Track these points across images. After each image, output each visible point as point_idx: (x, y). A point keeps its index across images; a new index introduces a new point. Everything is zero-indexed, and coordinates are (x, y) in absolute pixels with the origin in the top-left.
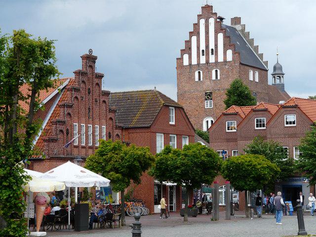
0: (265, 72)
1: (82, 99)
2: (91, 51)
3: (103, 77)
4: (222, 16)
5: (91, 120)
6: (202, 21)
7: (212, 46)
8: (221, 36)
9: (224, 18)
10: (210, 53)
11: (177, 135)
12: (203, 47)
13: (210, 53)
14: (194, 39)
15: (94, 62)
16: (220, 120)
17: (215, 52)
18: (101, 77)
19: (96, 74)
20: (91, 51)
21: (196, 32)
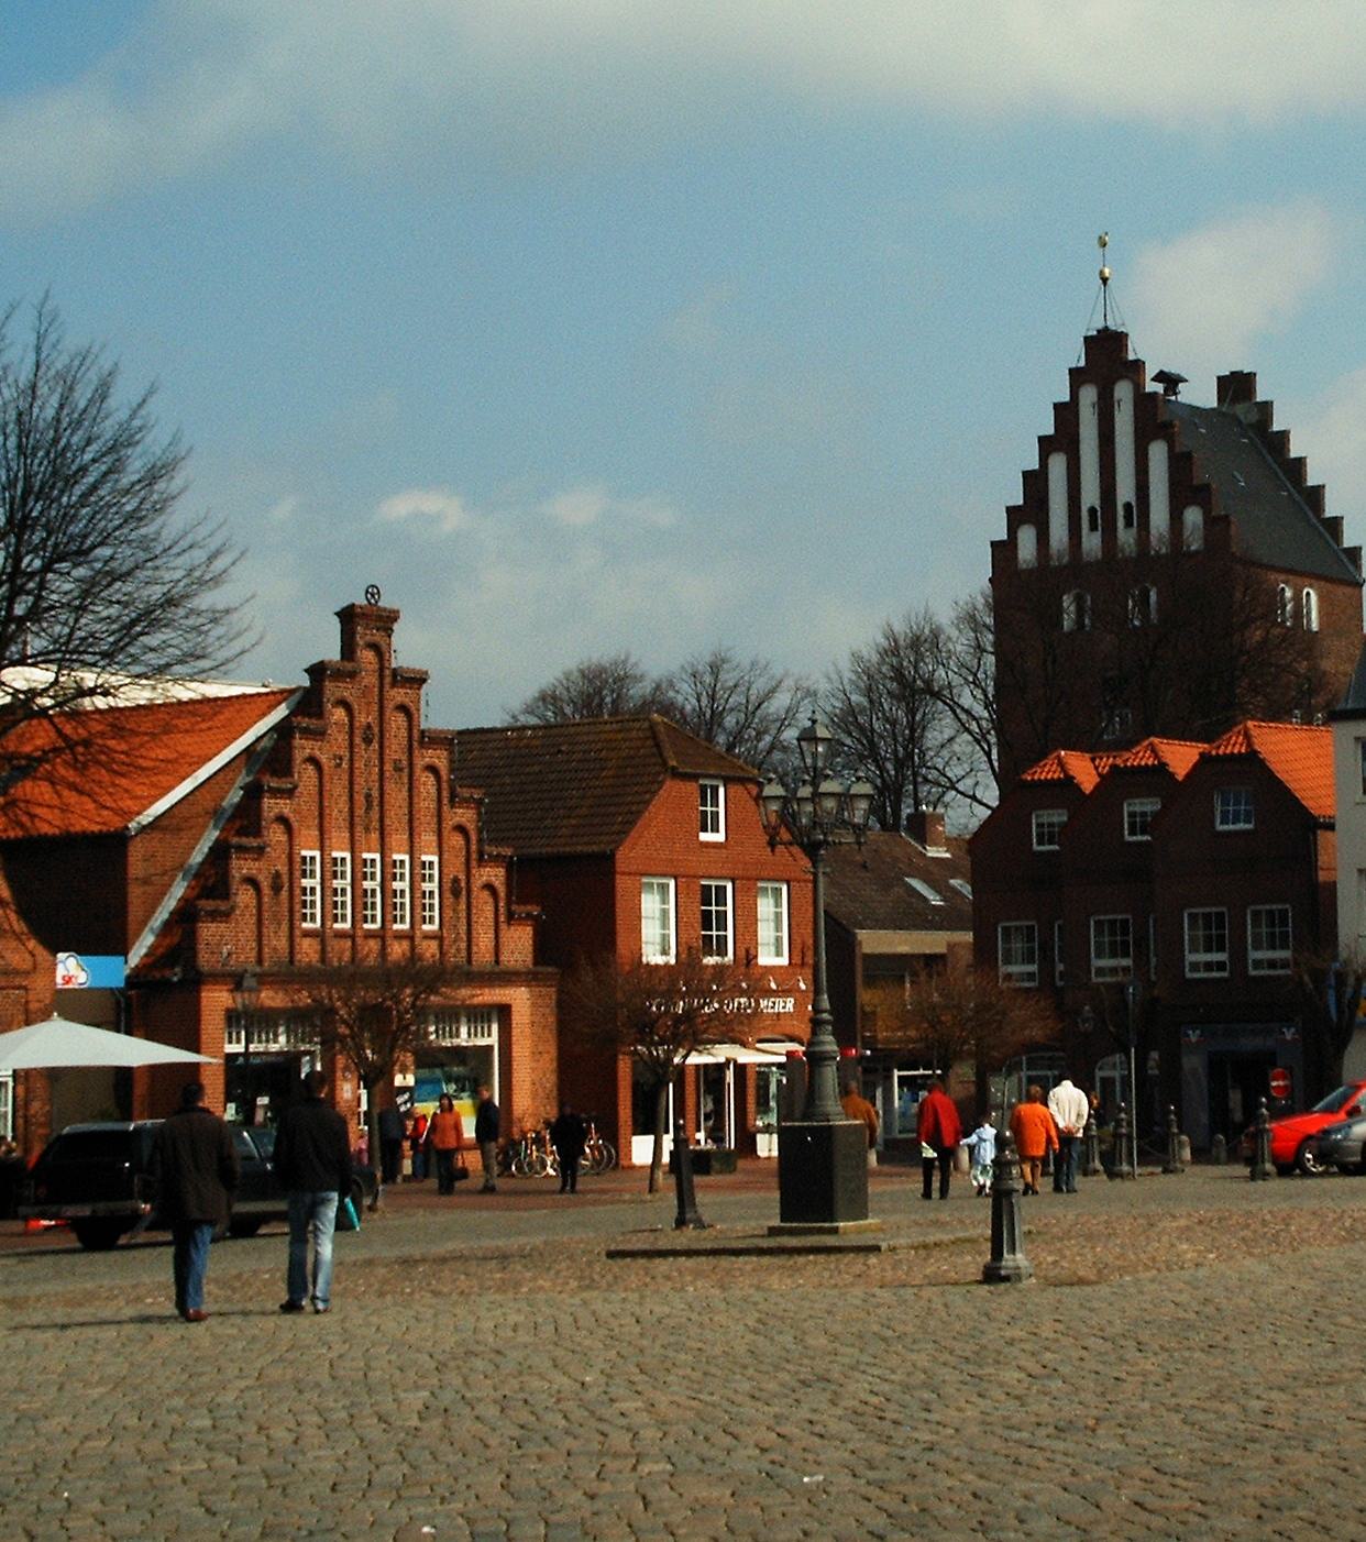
0: (1348, 590)
1: (339, 765)
2: (373, 592)
3: (424, 681)
4: (1172, 368)
5: (375, 836)
6: (1088, 395)
7: (1125, 492)
8: (1158, 452)
9: (1186, 377)
10: (1121, 523)
11: (676, 878)
12: (1090, 496)
13: (1121, 523)
14: (1058, 464)
15: (389, 631)
16: (445, 847)
17: (1140, 509)
18: (417, 680)
19: (395, 672)
20: (373, 592)
21: (1062, 439)
